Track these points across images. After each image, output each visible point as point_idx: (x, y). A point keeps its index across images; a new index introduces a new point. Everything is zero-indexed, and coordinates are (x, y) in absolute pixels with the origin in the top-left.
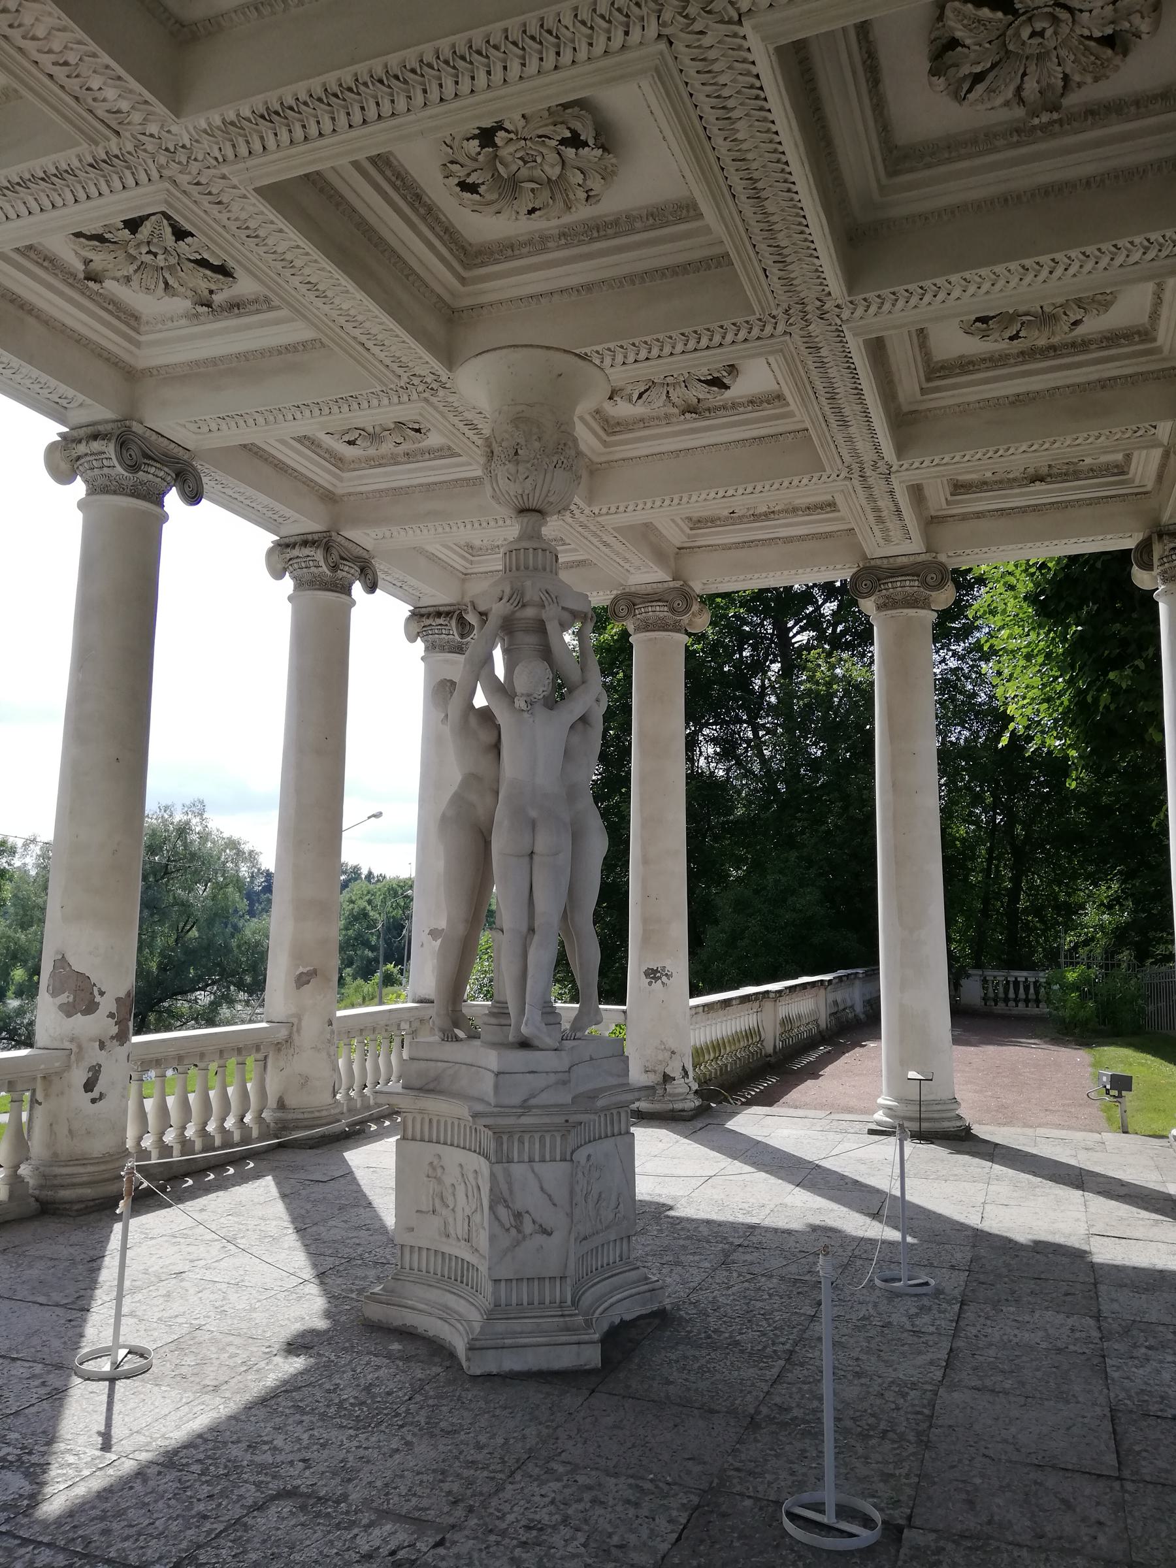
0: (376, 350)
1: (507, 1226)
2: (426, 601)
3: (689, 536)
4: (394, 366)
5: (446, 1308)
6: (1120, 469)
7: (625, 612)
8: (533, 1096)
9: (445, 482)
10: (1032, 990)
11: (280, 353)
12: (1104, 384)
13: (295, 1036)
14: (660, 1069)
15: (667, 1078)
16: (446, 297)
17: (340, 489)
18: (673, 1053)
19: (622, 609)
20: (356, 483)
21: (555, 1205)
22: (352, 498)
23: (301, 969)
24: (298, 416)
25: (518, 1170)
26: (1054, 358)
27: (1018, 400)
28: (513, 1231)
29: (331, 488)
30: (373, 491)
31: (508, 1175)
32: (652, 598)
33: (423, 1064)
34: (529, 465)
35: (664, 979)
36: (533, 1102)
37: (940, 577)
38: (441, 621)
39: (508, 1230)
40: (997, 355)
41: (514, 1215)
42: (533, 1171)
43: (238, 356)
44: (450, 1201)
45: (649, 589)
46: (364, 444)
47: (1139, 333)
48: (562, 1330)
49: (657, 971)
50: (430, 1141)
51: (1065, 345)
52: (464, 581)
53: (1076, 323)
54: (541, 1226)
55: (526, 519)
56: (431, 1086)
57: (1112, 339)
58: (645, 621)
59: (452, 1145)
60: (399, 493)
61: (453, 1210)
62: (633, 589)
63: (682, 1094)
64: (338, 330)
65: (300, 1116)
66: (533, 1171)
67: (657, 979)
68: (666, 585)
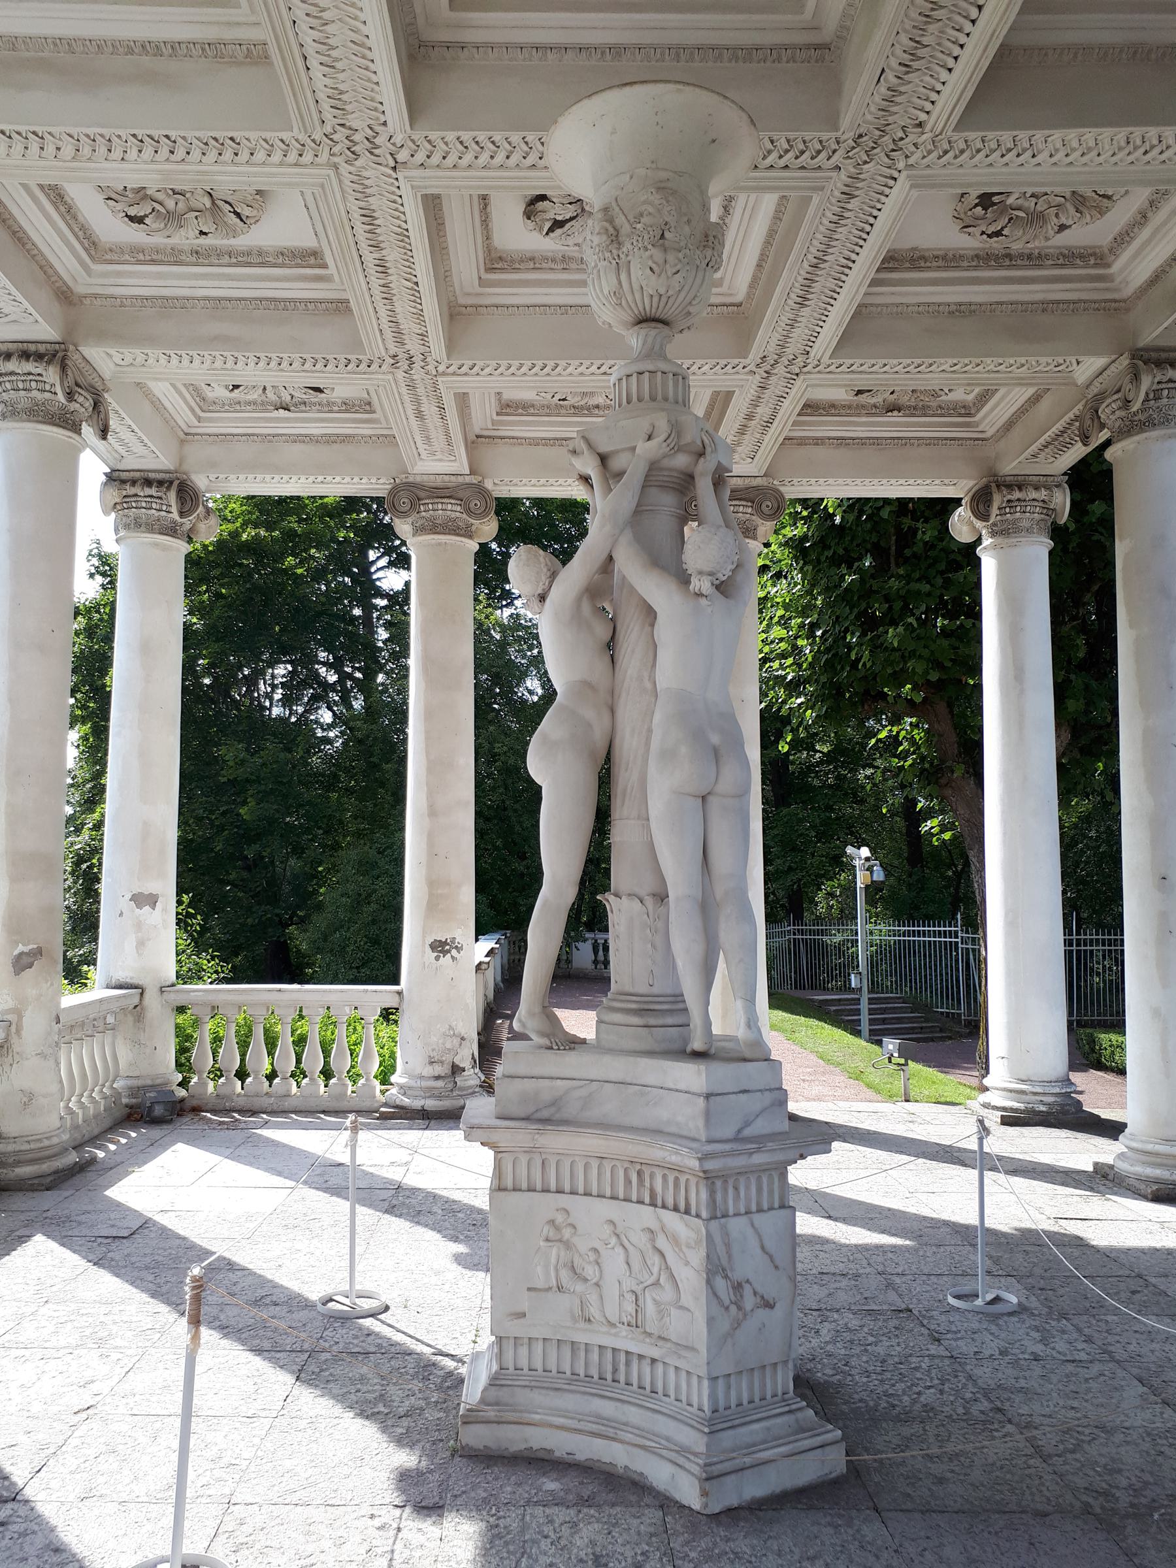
0: (317, 71)
1: (727, 1302)
2: (130, 463)
3: (493, 422)
4: (326, 105)
5: (599, 1418)
6: (966, 410)
7: (406, 507)
8: (747, 1124)
9: (244, 299)
10: (601, 953)
11: (130, 51)
12: (1046, 306)
13: (14, 1040)
14: (448, 1058)
15: (456, 1070)
16: (421, 21)
17: (82, 284)
18: (463, 1039)
19: (404, 502)
20: (112, 281)
21: (776, 1267)
22: (98, 302)
23: (21, 948)
24: (133, 154)
25: (737, 1226)
26: (1009, 267)
27: (961, 311)
28: (733, 1308)
29: (70, 284)
30: (132, 297)
31: (726, 1234)
32: (441, 492)
33: (529, 1085)
34: (680, 255)
35: (454, 952)
36: (747, 1132)
37: (776, 505)
38: (153, 491)
39: (727, 1308)
40: (950, 255)
41: (734, 1288)
42: (753, 1225)
43: (57, 42)
44: (590, 1271)
45: (439, 483)
46: (155, 226)
47: (1094, 254)
48: (797, 1433)
49: (446, 943)
50: (546, 1190)
51: (1021, 256)
52: (182, 442)
53: (1062, 228)
54: (762, 1297)
55: (651, 332)
56: (545, 1114)
57: (1070, 257)
58: (432, 520)
59: (587, 1194)
60: (166, 305)
61: (597, 1284)
62: (418, 479)
63: (471, 1087)
64: (289, 24)
65: (26, 1147)
66: (753, 1225)
67: (445, 953)
68: (460, 479)
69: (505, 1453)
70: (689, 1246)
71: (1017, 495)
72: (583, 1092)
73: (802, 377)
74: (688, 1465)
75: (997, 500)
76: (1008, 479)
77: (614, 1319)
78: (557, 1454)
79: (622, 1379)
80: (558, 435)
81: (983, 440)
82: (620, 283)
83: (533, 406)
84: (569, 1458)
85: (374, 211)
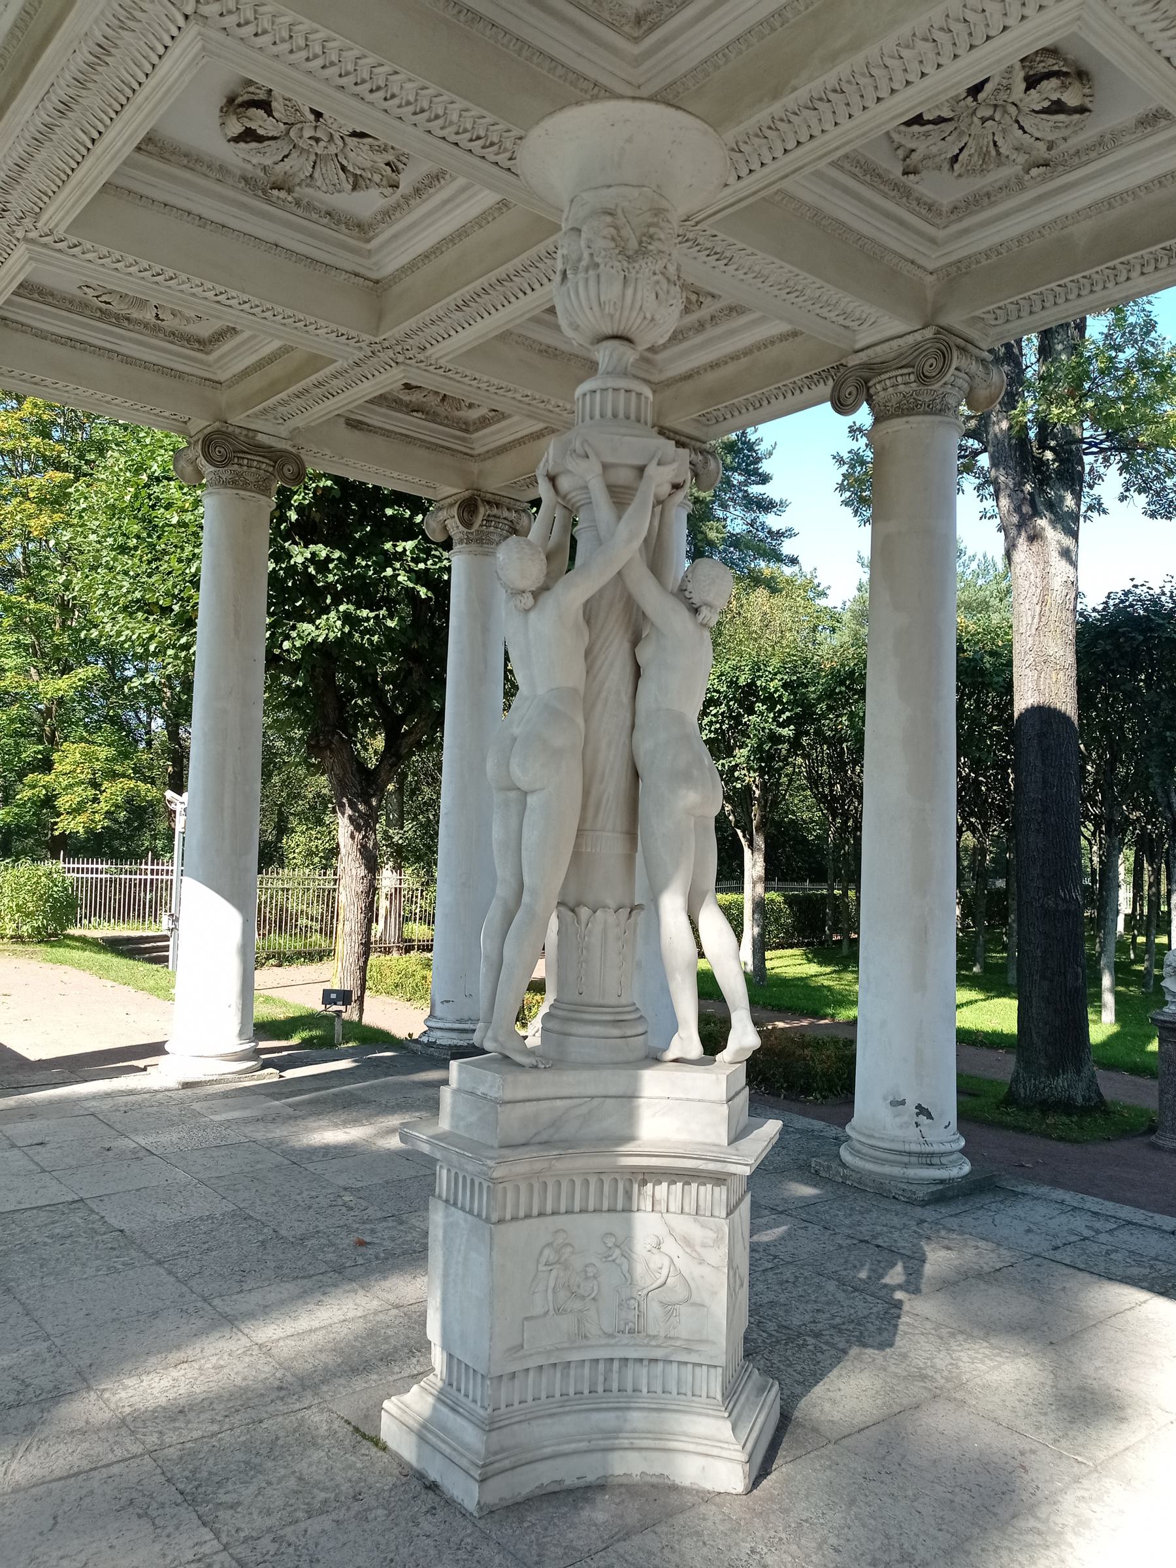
6: (467, 427)
33: (530, 1107)
37: (296, 470)
56: (545, 1136)
69: (519, 1499)
70: (704, 1246)
71: (495, 511)
72: (584, 1110)
73: (402, 367)
74: (724, 1454)
75: (482, 511)
76: (488, 495)
77: (609, 1330)
78: (567, 1482)
79: (615, 1387)
80: (73, 335)
81: (471, 456)
82: (624, 295)
83: (52, 295)
84: (582, 1483)
85: (116, 46)
